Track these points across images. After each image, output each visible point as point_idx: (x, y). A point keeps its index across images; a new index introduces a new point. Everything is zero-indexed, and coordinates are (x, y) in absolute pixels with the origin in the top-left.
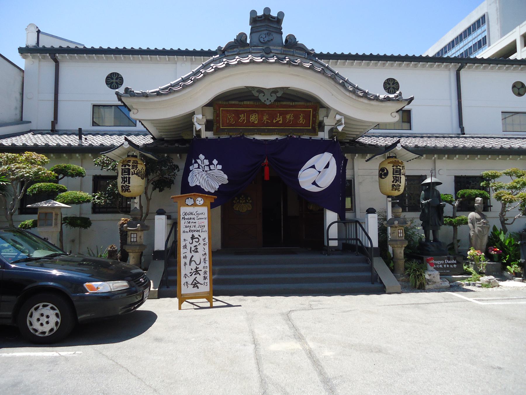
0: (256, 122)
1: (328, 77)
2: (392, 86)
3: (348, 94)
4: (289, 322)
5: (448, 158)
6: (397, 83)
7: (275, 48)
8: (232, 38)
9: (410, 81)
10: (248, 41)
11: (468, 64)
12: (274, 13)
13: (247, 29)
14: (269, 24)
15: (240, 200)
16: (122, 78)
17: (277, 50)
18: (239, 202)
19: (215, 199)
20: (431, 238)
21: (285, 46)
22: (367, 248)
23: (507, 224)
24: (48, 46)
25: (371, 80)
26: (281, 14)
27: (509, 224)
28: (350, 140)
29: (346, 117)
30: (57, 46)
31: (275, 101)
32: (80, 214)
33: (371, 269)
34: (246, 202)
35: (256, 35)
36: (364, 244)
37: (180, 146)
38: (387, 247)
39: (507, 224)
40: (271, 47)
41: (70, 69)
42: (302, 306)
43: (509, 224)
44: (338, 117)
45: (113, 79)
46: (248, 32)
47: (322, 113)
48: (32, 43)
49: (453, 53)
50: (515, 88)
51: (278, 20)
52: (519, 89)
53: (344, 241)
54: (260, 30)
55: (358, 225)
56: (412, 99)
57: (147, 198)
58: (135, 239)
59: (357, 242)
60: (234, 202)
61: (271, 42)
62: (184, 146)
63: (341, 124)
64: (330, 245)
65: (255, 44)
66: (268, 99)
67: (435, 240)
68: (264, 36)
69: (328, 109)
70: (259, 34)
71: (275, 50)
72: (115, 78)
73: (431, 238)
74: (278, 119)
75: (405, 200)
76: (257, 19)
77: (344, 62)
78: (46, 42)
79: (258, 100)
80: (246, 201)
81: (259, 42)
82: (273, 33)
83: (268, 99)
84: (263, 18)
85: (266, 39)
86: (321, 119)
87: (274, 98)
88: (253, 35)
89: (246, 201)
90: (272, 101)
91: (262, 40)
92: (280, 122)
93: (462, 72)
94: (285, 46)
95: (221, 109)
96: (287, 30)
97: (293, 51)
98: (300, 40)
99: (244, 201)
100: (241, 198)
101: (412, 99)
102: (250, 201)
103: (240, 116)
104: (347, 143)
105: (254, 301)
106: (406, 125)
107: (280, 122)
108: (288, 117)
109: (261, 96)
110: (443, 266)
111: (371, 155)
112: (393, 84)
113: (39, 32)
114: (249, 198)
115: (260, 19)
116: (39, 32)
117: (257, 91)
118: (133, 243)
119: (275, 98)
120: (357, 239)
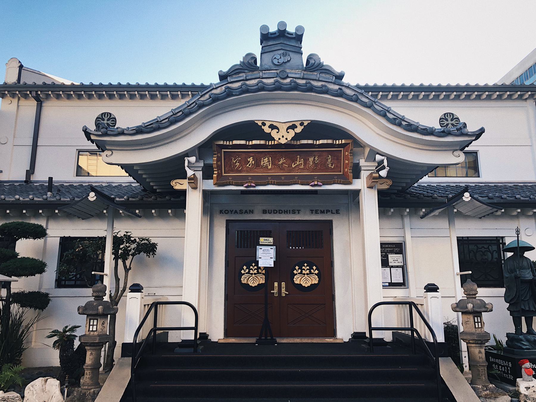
0: (270, 167)
1: (499, 216)
7: (293, 71)
8: (237, 60)
10: (258, 64)
12: (291, 29)
13: (256, 50)
15: (250, 269)
16: (115, 118)
17: (296, 74)
20: (525, 330)
22: (429, 343)
24: (30, 82)
25: (428, 115)
26: (300, 29)
28: (398, 190)
29: (391, 160)
30: (39, 82)
31: (293, 139)
32: (40, 288)
35: (268, 57)
36: (423, 337)
37: (172, 199)
38: (458, 345)
40: (288, 71)
41: (55, 111)
44: (378, 157)
45: (104, 120)
46: (258, 54)
48: (12, 79)
51: (299, 38)
54: (273, 49)
56: (482, 131)
57: (125, 267)
58: (91, 323)
59: (413, 334)
60: (295, 272)
61: (288, 64)
63: (384, 168)
64: (373, 337)
65: (266, 67)
66: (283, 137)
67: (530, 331)
68: (278, 57)
70: (272, 54)
71: (293, 73)
72: (106, 119)
73: (525, 330)
74: (298, 163)
76: (270, 36)
79: (269, 137)
80: (310, 272)
81: (272, 64)
82: (290, 53)
83: (283, 137)
85: (281, 61)
87: (292, 133)
88: (264, 55)
89: (310, 272)
90: (289, 139)
91: (276, 62)
96: (308, 48)
98: (326, 61)
101: (482, 131)
102: (317, 272)
103: (249, 160)
104: (394, 194)
109: (274, 133)
113: (21, 67)
114: (314, 268)
115: (273, 36)
116: (21, 67)
117: (269, 127)
119: (293, 134)
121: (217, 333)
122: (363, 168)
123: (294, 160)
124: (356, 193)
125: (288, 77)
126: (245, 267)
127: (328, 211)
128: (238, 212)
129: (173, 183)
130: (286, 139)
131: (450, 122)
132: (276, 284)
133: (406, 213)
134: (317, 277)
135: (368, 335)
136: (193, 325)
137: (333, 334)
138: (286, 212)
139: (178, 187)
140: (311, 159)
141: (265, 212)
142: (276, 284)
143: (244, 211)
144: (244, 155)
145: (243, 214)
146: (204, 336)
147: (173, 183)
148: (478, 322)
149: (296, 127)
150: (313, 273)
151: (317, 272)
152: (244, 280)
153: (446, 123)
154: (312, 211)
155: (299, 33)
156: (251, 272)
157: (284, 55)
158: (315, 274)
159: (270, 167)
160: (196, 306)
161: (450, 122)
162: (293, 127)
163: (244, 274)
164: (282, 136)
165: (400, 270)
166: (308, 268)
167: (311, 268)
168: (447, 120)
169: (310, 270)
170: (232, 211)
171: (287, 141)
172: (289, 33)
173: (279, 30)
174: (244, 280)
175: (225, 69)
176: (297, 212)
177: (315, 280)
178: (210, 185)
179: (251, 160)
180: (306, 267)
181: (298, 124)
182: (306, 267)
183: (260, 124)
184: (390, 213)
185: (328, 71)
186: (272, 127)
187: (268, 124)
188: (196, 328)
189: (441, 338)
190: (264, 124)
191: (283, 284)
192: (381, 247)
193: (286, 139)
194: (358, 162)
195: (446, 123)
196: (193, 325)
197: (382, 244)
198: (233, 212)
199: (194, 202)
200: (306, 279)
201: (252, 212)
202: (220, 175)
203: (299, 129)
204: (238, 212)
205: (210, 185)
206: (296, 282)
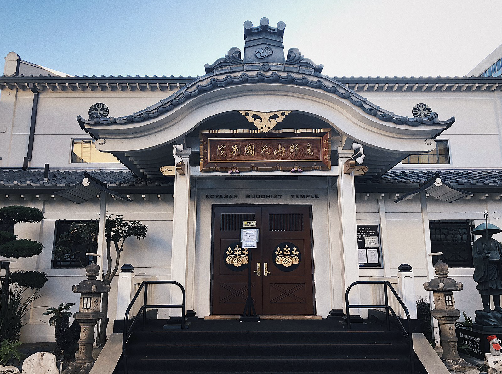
0: (253, 155)
9: (442, 106)
10: (242, 58)
12: (273, 24)
19: (500, 243)
21: (287, 63)
22: (402, 320)
24: (27, 75)
28: (373, 176)
29: (367, 148)
30: (36, 75)
31: (275, 128)
32: (36, 269)
34: (291, 254)
35: (251, 51)
36: (397, 314)
41: (51, 102)
44: (355, 145)
48: (11, 72)
51: (280, 33)
56: (452, 121)
58: (89, 305)
61: (270, 58)
62: (166, 185)
63: (360, 155)
64: (350, 314)
65: (250, 60)
66: (265, 126)
68: (261, 51)
70: (255, 48)
72: (99, 109)
74: (279, 151)
78: (25, 72)
79: (252, 126)
80: (291, 253)
82: (272, 48)
83: (265, 126)
84: (260, 30)
87: (274, 123)
88: (247, 50)
94: (287, 63)
96: (288, 43)
97: (299, 73)
98: (306, 54)
99: (289, 253)
101: (452, 121)
102: (297, 253)
103: (233, 148)
104: (370, 179)
106: (442, 159)
108: (292, 147)
109: (257, 123)
110: (361, 232)
111: (402, 194)
113: (19, 60)
114: (295, 249)
115: (256, 31)
116: (19, 60)
117: (253, 117)
118: (86, 311)
120: (387, 307)
121: (203, 310)
122: (340, 156)
123: (276, 148)
125: (270, 70)
126: (229, 249)
129: (162, 170)
130: (269, 128)
131: (422, 112)
132: (259, 265)
133: (381, 198)
135: (345, 312)
136: (181, 303)
137: (313, 311)
138: (268, 197)
139: (166, 173)
140: (292, 147)
141: (248, 197)
142: (259, 265)
143: (228, 196)
144: (229, 143)
145: (228, 199)
146: (191, 313)
147: (162, 170)
149: (278, 117)
152: (229, 261)
153: (418, 113)
156: (236, 253)
157: (266, 49)
159: (253, 155)
160: (184, 285)
161: (422, 112)
162: (275, 117)
164: (265, 126)
170: (217, 196)
172: (271, 29)
174: (229, 261)
175: (211, 63)
178: (196, 171)
179: (235, 147)
180: (287, 249)
181: (279, 114)
182: (287, 249)
183: (244, 114)
184: (366, 198)
185: (307, 64)
186: (255, 117)
187: (251, 114)
188: (183, 306)
190: (247, 114)
191: (266, 265)
193: (269, 128)
195: (418, 113)
196: (181, 303)
199: (182, 187)
200: (287, 259)
201: (236, 196)
202: (206, 162)
203: (280, 119)
205: (196, 171)
206: (278, 263)
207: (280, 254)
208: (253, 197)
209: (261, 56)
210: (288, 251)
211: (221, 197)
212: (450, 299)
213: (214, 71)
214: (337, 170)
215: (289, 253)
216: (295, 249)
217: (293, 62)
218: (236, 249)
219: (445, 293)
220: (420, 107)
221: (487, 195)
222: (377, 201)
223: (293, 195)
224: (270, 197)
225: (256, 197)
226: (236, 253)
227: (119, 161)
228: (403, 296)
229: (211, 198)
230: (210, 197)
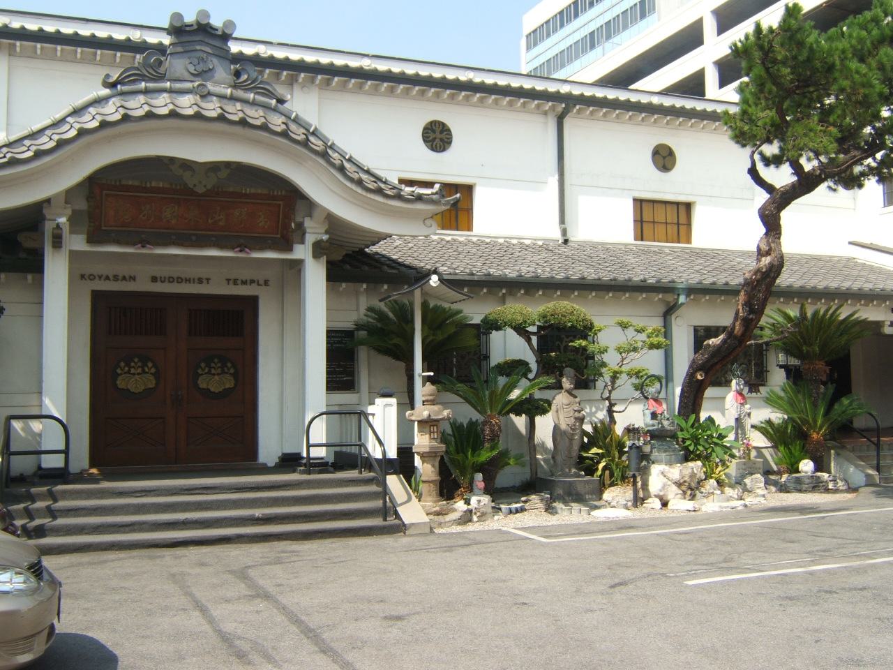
2: (438, 133)
3: (349, 184)
4: (246, 581)
5: (526, 293)
6: (449, 130)
11: (578, 107)
12: (217, 21)
14: (206, 40)
15: (130, 367)
18: (129, 372)
23: (617, 412)
27: (620, 412)
28: (353, 252)
33: (385, 492)
39: (617, 412)
42: (263, 559)
43: (620, 412)
47: (300, 205)
49: (242, 588)
50: (656, 156)
52: (664, 158)
53: (338, 449)
55: (362, 418)
58: (432, 430)
66: (200, 182)
69: (310, 205)
75: (452, 370)
77: (346, 82)
83: (200, 182)
84: (195, 27)
86: (299, 219)
92: (221, 223)
93: (567, 122)
95: (105, 192)
99: (139, 370)
100: (133, 364)
102: (153, 370)
105: (176, 558)
107: (221, 223)
112: (441, 132)
115: (188, 29)
122: (308, 230)
124: (298, 265)
126: (122, 364)
127: (252, 282)
128: (111, 278)
130: (205, 186)
133: (362, 290)
134: (232, 378)
135: (305, 455)
136: (62, 447)
141: (154, 279)
143: (120, 278)
145: (119, 282)
148: (434, 432)
149: (220, 170)
150: (147, 373)
151: (232, 371)
152: (121, 383)
153: (438, 130)
154: (228, 280)
155: (228, 32)
156: (213, 371)
158: (151, 374)
160: (65, 421)
163: (121, 374)
165: (63, 455)
166: (139, 364)
167: (144, 365)
168: (434, 139)
169: (142, 367)
170: (100, 277)
171: (205, 190)
172: (211, 28)
173: (198, 23)
174: (121, 383)
176: (205, 281)
177: (229, 383)
184: (341, 289)
188: (66, 452)
189: (392, 454)
192: (328, 337)
193: (205, 186)
194: (301, 220)
195: (438, 130)
196: (62, 447)
197: (328, 332)
198: (102, 279)
201: (133, 278)
204: (111, 278)
206: (201, 386)
207: (206, 373)
208: (163, 279)
209: (195, 70)
210: (139, 367)
211: (107, 278)
212: (435, 430)
213: (119, 87)
214: (302, 252)
215: (139, 370)
216: (150, 365)
217: (245, 86)
218: (213, 365)
219: (430, 424)
220: (435, 125)
221: (504, 291)
222: (357, 294)
223: (228, 280)
224: (192, 282)
225: (167, 280)
226: (213, 371)
227: (464, 401)
228: (367, 386)
229: (91, 280)
230: (87, 278)
